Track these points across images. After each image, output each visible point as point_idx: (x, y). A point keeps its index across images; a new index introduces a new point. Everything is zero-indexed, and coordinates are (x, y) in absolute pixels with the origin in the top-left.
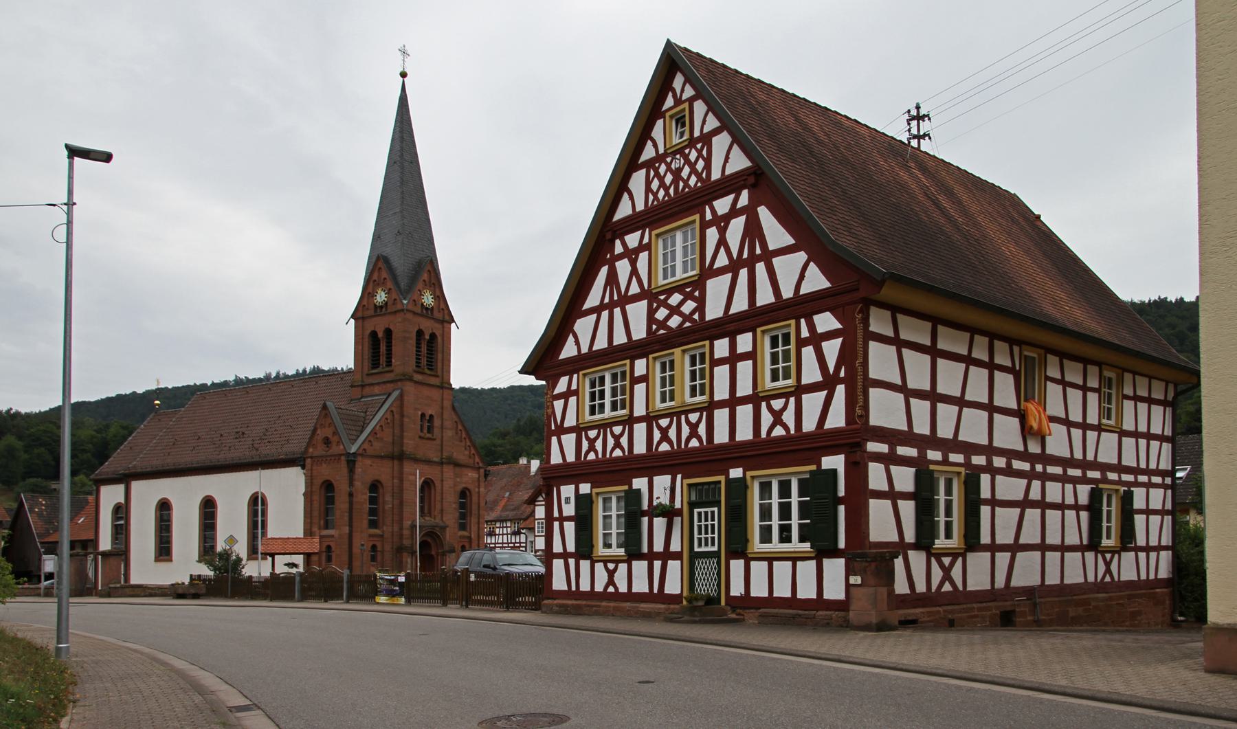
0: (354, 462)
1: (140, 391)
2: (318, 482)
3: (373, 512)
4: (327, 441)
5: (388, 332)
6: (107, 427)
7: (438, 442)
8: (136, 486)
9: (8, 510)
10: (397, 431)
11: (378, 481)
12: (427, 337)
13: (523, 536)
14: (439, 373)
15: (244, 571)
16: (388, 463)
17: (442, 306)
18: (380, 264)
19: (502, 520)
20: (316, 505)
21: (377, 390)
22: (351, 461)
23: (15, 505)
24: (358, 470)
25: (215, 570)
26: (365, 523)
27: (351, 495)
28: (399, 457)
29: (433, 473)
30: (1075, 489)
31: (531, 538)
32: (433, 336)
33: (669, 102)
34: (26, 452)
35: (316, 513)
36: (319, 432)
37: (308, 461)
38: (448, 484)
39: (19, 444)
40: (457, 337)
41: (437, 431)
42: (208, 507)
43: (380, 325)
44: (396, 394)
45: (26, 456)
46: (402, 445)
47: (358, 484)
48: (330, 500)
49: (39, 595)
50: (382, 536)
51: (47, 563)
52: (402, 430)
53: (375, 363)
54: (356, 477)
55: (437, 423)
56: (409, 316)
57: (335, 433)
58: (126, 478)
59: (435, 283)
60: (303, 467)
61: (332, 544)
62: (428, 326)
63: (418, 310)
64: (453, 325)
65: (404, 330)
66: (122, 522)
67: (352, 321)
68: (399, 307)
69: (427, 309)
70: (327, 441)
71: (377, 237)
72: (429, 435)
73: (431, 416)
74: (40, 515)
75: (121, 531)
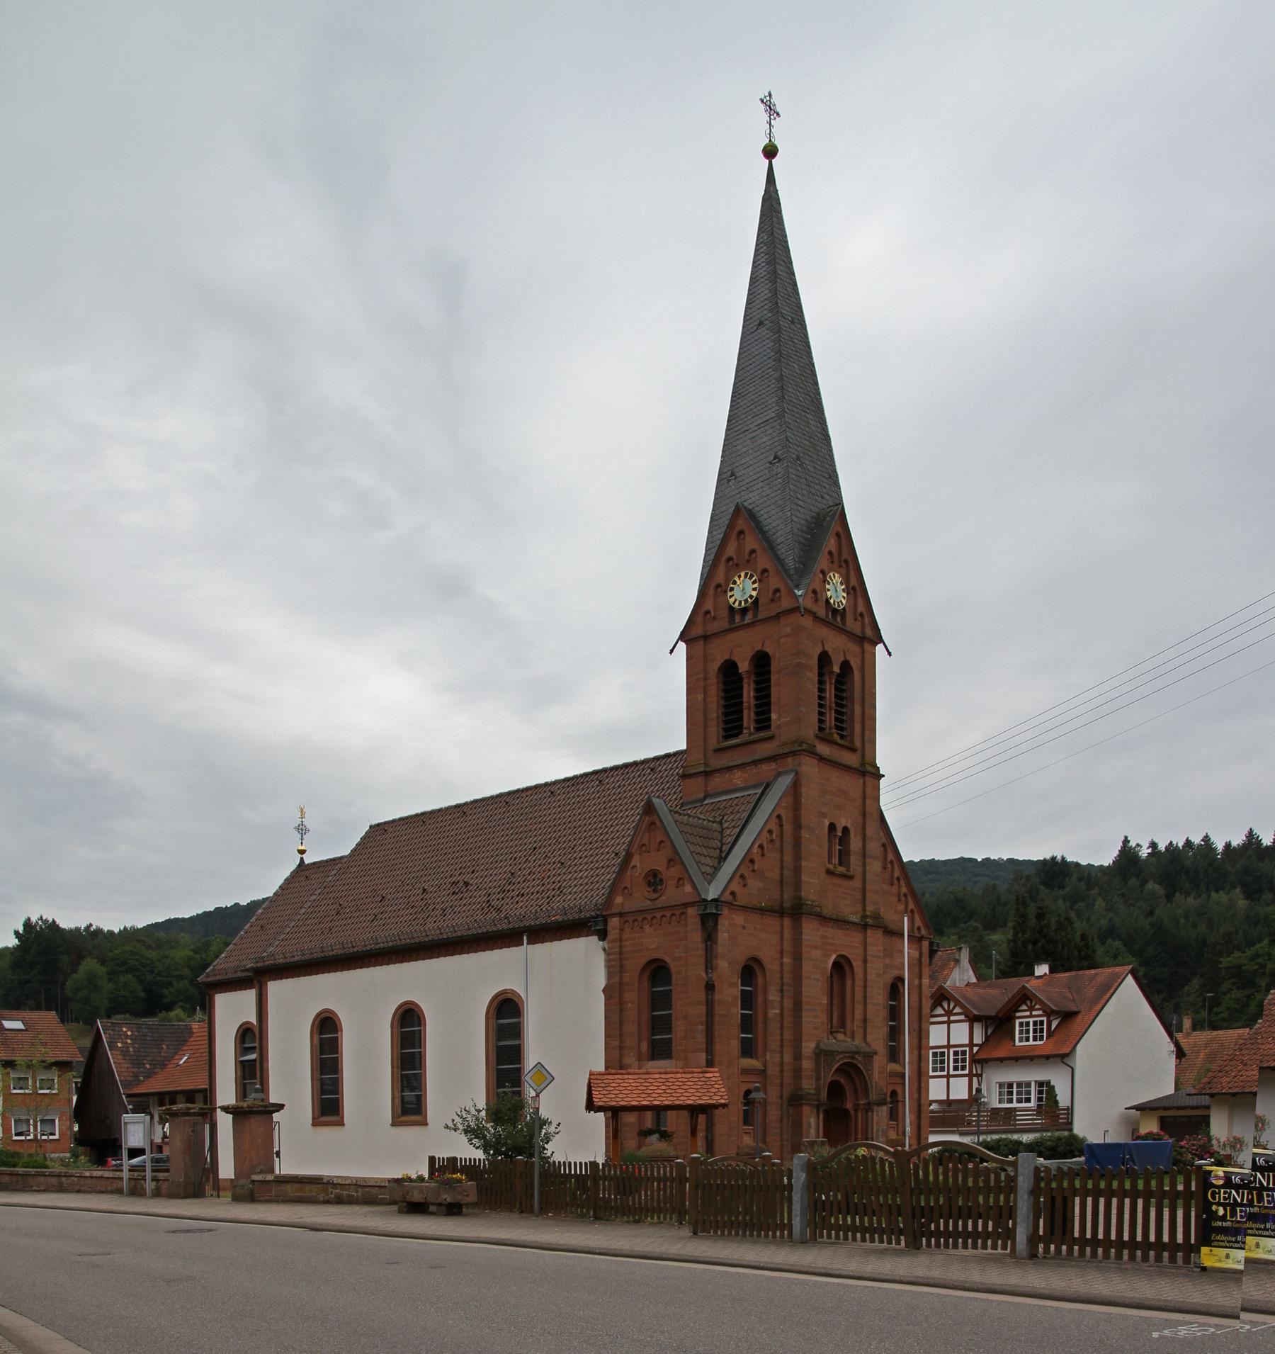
0: (716, 916)
1: (244, 902)
2: (635, 964)
3: (747, 1024)
4: (654, 880)
5: (762, 662)
6: (207, 944)
7: (857, 883)
8: (277, 989)
9: (81, 1050)
10: (788, 859)
11: (756, 960)
12: (836, 669)
14: (858, 744)
15: (550, 1147)
16: (772, 923)
17: (861, 608)
18: (741, 524)
21: (738, 778)
22: (709, 917)
23: (87, 1043)
24: (723, 936)
25: (485, 1147)
26: (735, 1045)
27: (710, 987)
28: (794, 911)
29: (847, 942)
32: (846, 666)
34: (110, 980)
35: (631, 1028)
36: (636, 861)
37: (614, 922)
38: (875, 967)
39: (102, 970)
40: (890, 676)
41: (854, 860)
42: (409, 1022)
43: (742, 650)
44: (785, 782)
45: (111, 985)
46: (798, 885)
47: (722, 964)
48: (661, 1001)
49: (119, 1192)
50: (763, 1073)
51: (131, 1128)
52: (798, 857)
53: (732, 726)
54: (720, 949)
55: (855, 844)
56: (807, 622)
57: (674, 860)
58: (257, 978)
59: (848, 563)
60: (603, 935)
62: (837, 645)
63: (821, 612)
64: (880, 647)
65: (797, 649)
66: (253, 1056)
67: (682, 646)
68: (786, 604)
69: (835, 611)
70: (654, 880)
71: (727, 475)
72: (841, 869)
73: (846, 830)
74: (124, 1052)
75: (252, 1072)
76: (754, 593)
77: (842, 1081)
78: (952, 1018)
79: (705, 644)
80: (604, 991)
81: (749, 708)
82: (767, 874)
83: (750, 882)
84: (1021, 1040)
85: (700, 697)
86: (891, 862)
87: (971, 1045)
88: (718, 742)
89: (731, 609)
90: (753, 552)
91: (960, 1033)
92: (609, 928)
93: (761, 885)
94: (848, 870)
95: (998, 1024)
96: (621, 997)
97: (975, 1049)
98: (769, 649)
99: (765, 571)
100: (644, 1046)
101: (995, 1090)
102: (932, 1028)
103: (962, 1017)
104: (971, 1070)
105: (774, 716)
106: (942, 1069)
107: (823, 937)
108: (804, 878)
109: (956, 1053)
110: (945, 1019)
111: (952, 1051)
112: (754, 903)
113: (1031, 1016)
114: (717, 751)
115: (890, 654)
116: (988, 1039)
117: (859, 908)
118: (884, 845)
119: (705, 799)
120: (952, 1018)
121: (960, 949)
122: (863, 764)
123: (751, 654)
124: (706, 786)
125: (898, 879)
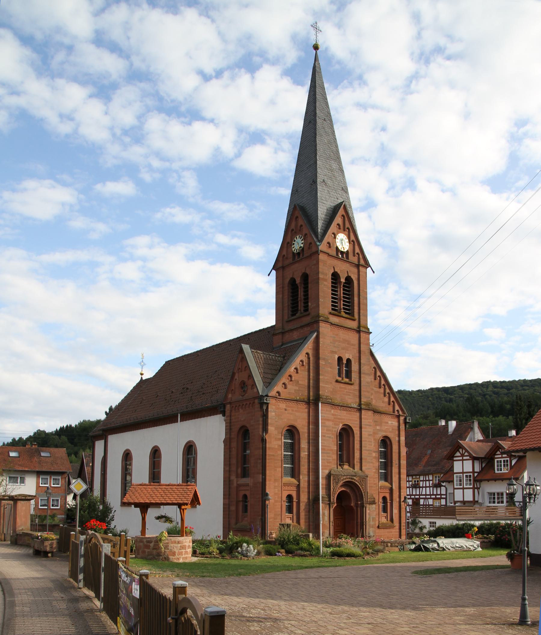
2: (236, 428)
7: (357, 387)
11: (294, 427)
12: (343, 280)
13: (443, 489)
17: (357, 250)
19: (425, 474)
20: (234, 452)
24: (271, 414)
30: (143, 532)
31: (450, 491)
32: (349, 280)
33: (418, 477)
35: (234, 461)
36: (236, 377)
37: (228, 407)
53: (294, 310)
55: (355, 367)
61: (248, 493)
62: (344, 270)
67: (274, 272)
69: (342, 253)
73: (349, 361)
76: (302, 245)
77: (348, 491)
78: (464, 458)
79: (283, 271)
80: (224, 442)
81: (301, 301)
82: (300, 382)
83: (289, 386)
84: (498, 470)
85: (281, 296)
86: (379, 376)
87: (474, 472)
88: (288, 318)
89: (293, 253)
90: (301, 226)
91: (468, 466)
92: (226, 410)
93: (297, 388)
94: (351, 381)
95: (487, 461)
96: (230, 445)
97: (476, 474)
98: (308, 272)
99: (306, 234)
100: (239, 470)
101: (487, 497)
102: (455, 462)
103: (468, 458)
104: (474, 486)
105: (310, 304)
106: (460, 485)
107: (333, 415)
108: (321, 384)
109: (466, 476)
110: (461, 458)
111: (464, 475)
112: (293, 397)
113: (502, 457)
114: (287, 322)
115: (374, 272)
116: (482, 469)
117: (358, 400)
118: (374, 368)
119: (282, 345)
120: (464, 458)
121: (473, 422)
122: (359, 327)
123: (301, 275)
124: (282, 339)
125: (383, 385)
